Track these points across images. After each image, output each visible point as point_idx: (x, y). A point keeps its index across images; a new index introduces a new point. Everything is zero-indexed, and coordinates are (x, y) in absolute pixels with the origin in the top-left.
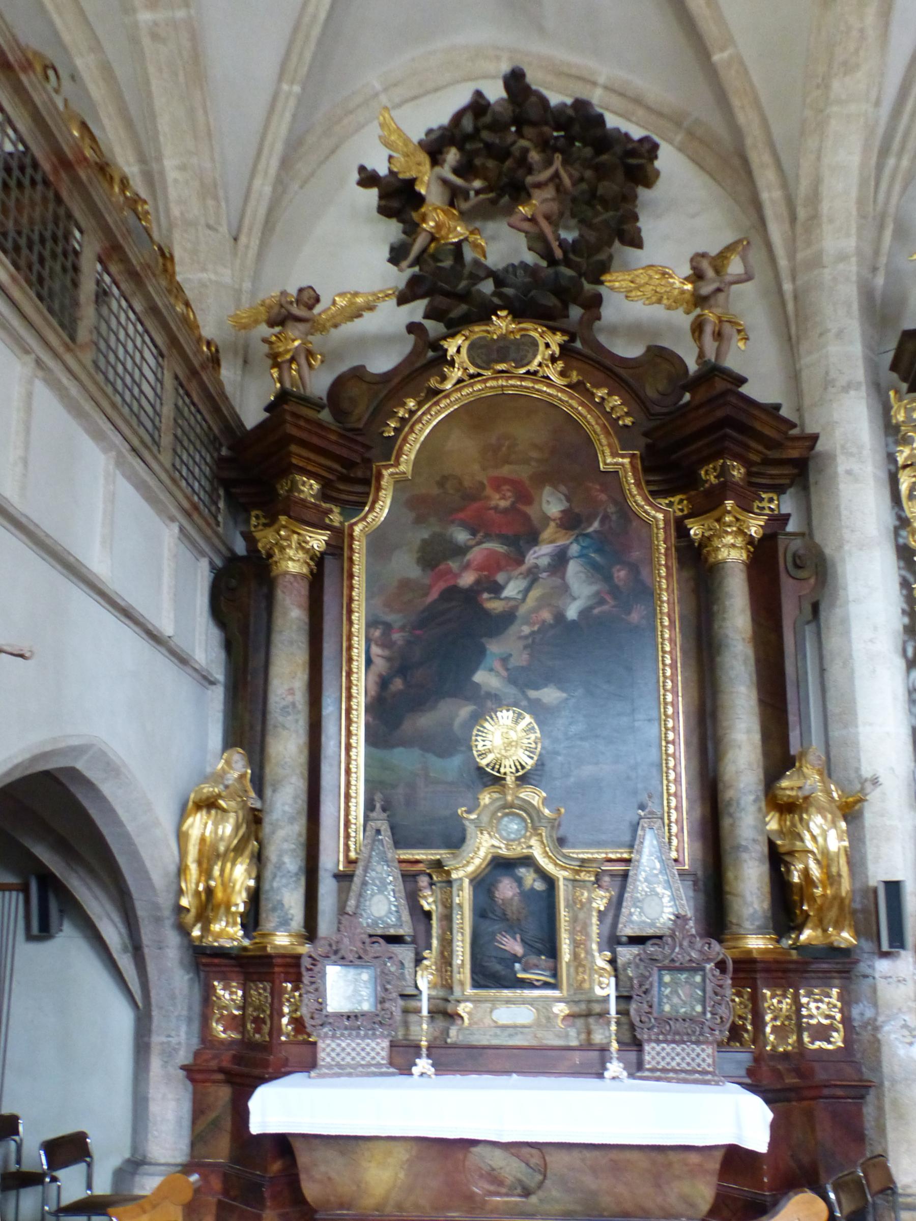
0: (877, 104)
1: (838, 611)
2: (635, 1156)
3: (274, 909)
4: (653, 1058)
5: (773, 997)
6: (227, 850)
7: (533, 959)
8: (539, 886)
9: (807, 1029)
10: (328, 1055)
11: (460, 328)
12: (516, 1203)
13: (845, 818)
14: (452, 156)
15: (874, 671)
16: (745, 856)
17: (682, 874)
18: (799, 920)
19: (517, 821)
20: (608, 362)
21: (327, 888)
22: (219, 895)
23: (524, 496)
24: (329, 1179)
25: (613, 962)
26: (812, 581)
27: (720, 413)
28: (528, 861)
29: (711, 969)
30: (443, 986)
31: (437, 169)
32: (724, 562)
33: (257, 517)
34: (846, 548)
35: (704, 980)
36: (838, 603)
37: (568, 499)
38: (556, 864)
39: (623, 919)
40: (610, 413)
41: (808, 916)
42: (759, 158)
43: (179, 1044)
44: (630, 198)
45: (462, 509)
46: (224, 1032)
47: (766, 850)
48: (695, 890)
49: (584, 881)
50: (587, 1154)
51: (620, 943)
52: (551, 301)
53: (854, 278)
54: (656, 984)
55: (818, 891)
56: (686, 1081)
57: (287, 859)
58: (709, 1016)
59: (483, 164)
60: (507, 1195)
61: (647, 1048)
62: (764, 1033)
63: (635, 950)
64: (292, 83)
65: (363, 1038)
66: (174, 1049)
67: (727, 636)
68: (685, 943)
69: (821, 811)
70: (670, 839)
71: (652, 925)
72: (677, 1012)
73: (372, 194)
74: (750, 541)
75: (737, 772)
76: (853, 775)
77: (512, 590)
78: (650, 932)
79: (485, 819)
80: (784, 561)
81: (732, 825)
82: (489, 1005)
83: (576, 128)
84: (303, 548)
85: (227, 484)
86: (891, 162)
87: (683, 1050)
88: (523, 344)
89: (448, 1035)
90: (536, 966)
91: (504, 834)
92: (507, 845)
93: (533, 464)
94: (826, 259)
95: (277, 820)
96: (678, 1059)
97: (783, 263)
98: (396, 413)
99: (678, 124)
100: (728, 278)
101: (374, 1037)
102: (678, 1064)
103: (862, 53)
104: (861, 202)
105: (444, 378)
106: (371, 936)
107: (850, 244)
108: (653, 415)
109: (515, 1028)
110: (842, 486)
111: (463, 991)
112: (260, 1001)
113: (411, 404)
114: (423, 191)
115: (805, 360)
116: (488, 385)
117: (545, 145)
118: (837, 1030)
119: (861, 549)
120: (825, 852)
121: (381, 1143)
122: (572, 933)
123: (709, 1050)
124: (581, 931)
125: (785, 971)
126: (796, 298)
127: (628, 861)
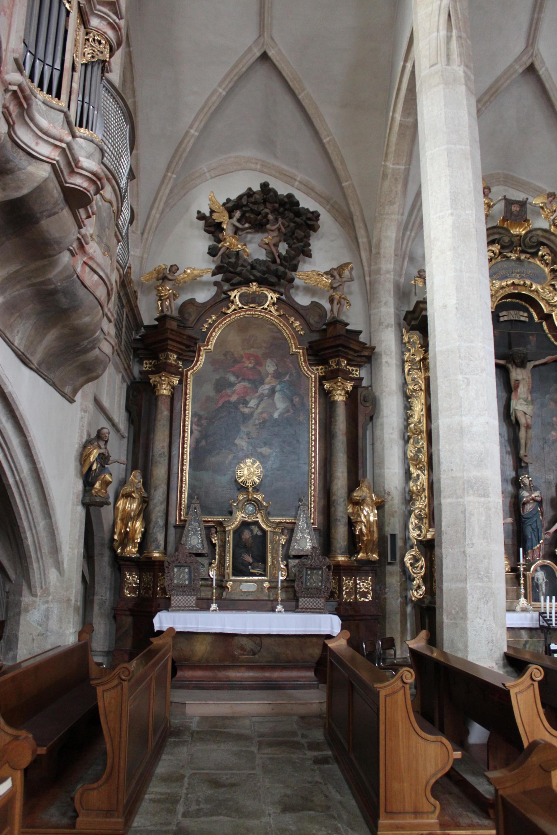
2: (294, 639)
3: (154, 541)
5: (346, 580)
6: (134, 516)
7: (256, 564)
8: (259, 533)
9: (358, 593)
10: (175, 602)
12: (250, 658)
13: (377, 509)
14: (238, 214)
15: (391, 447)
16: (339, 523)
17: (315, 529)
18: (358, 549)
21: (172, 531)
23: (259, 363)
24: (182, 649)
25: (287, 566)
27: (338, 342)
28: (256, 523)
30: (220, 575)
31: (231, 220)
32: (337, 401)
33: (146, 364)
34: (384, 394)
37: (277, 365)
38: (267, 525)
39: (291, 548)
40: (295, 329)
41: (361, 548)
42: (359, 224)
43: (106, 599)
44: (308, 237)
46: (129, 594)
47: (347, 521)
48: (319, 536)
51: (289, 558)
52: (273, 279)
53: (392, 281)
54: (305, 575)
55: (365, 538)
57: (159, 520)
59: (249, 216)
60: (247, 655)
61: (300, 600)
62: (342, 594)
63: (297, 561)
65: (187, 595)
68: (316, 558)
69: (368, 505)
71: (302, 550)
73: (202, 223)
74: (347, 392)
76: (382, 489)
77: (252, 403)
78: (302, 553)
79: (240, 505)
80: (360, 398)
81: (335, 510)
83: (287, 206)
84: (170, 385)
85: (135, 350)
86: (408, 233)
89: (222, 595)
90: (258, 567)
91: (247, 511)
92: (248, 517)
93: (263, 348)
94: (382, 272)
96: (311, 604)
97: (366, 268)
100: (344, 279)
101: (191, 595)
103: (396, 199)
104: (396, 250)
105: (229, 308)
106: (190, 553)
107: (391, 266)
110: (383, 368)
111: (229, 577)
114: (225, 227)
115: (373, 312)
117: (274, 211)
118: (370, 594)
120: (368, 521)
122: (272, 553)
123: (323, 600)
126: (370, 283)
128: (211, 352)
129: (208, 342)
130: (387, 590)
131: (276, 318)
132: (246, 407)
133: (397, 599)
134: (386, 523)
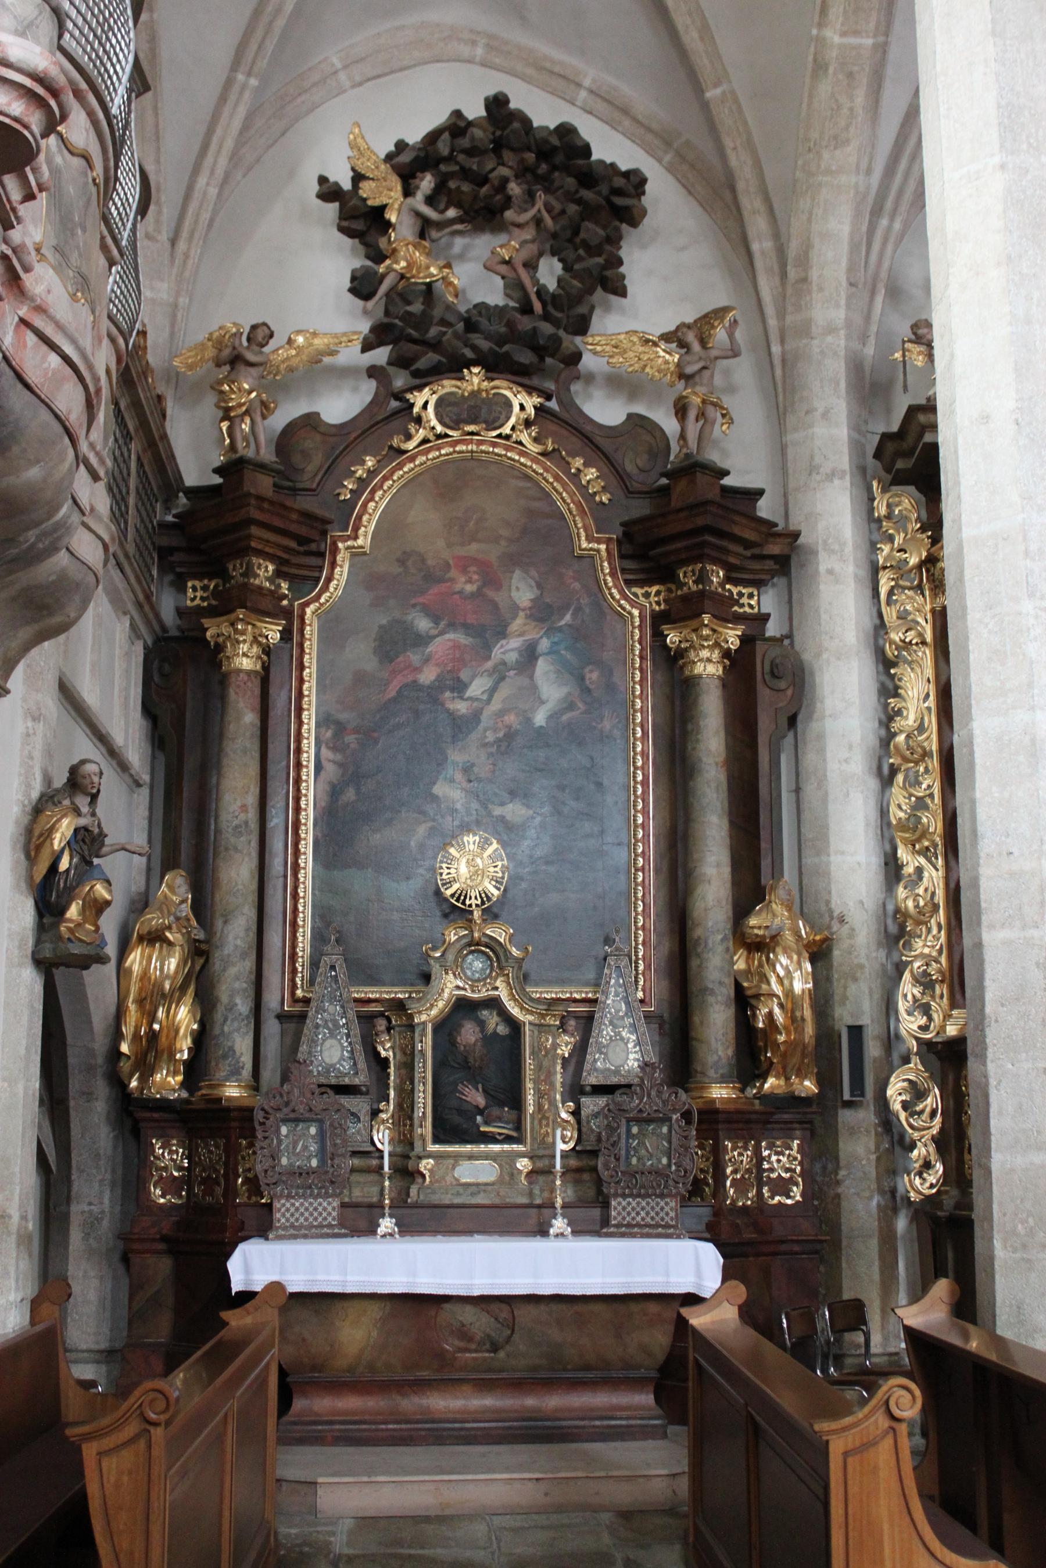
0: (869, 171)
1: (814, 725)
3: (225, 1057)
4: (619, 1213)
5: (734, 1149)
6: (172, 990)
7: (496, 1111)
8: (502, 1030)
9: (767, 1184)
10: (284, 1215)
11: (430, 379)
12: (485, 1359)
13: (813, 960)
14: (427, 183)
15: (848, 794)
16: (711, 999)
17: (648, 1016)
18: (765, 1066)
19: (483, 958)
20: (588, 428)
21: (272, 1028)
22: (163, 1041)
23: (491, 580)
24: (304, 1340)
25: (576, 1113)
26: (789, 692)
27: (700, 521)
28: (494, 1003)
29: (677, 1120)
30: (400, 1142)
31: (409, 200)
32: (700, 676)
34: (825, 656)
35: (670, 1131)
36: (815, 716)
37: (539, 586)
38: (522, 1008)
39: (587, 1066)
41: (772, 1063)
42: (751, 203)
43: (103, 1212)
44: (614, 240)
45: (423, 593)
46: (163, 1196)
49: (549, 1026)
50: (555, 1307)
51: (583, 1093)
52: (526, 357)
53: (842, 353)
55: (782, 1038)
56: (648, 1236)
57: (238, 1001)
58: (674, 1168)
59: (458, 188)
60: (476, 1351)
62: (725, 1186)
63: (602, 1101)
64: (249, 74)
65: (315, 1198)
66: (97, 1219)
67: (700, 760)
69: (786, 951)
70: (636, 978)
71: (617, 1072)
72: (644, 1165)
74: (726, 654)
75: (706, 910)
76: (823, 908)
77: (477, 688)
78: (614, 1080)
79: (450, 957)
80: (761, 667)
81: (700, 966)
82: (452, 1161)
83: (559, 158)
84: (260, 644)
85: (164, 553)
86: (884, 222)
87: (648, 1204)
88: (496, 403)
90: (500, 1119)
91: (469, 973)
92: (471, 986)
93: (503, 543)
94: (814, 329)
95: (229, 955)
96: (643, 1214)
97: (772, 322)
98: (355, 472)
99: (668, 144)
100: (714, 353)
102: (643, 1219)
103: (852, 130)
104: (851, 269)
105: (409, 437)
106: (320, 1086)
107: (839, 315)
108: (630, 492)
109: (477, 1187)
110: (822, 587)
112: (211, 1160)
113: (370, 462)
114: (393, 219)
115: (790, 437)
116: (457, 449)
117: (523, 172)
118: (797, 1184)
119: (839, 659)
120: (789, 993)
121: (357, 1304)
122: (536, 1082)
124: (545, 1081)
125: (748, 1122)
126: (784, 361)
127: (594, 1002)
128: (364, 554)
129: (356, 529)
130: (842, 1173)
131: (534, 460)
132: (462, 698)
133: (871, 1198)
134: (836, 998)
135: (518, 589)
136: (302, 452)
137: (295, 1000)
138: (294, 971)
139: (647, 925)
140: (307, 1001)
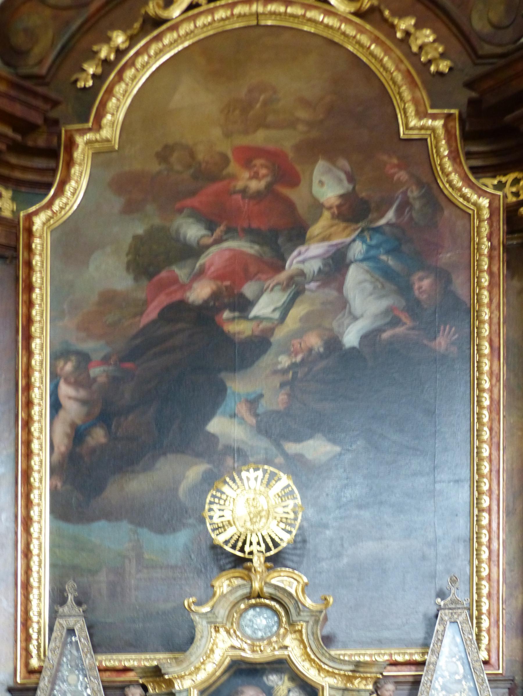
17: (493, 680)
37: (351, 179)
38: (320, 669)
45: (193, 193)
79: (222, 612)
91: (249, 631)
93: (301, 127)
98: (96, 53)
127: (422, 664)
128: (112, 151)
129: (99, 117)
131: (344, 19)
132: (246, 318)
135: (321, 183)
136: (26, 30)
137: (31, 672)
138: (28, 638)
139: (494, 576)
140: (39, 671)
